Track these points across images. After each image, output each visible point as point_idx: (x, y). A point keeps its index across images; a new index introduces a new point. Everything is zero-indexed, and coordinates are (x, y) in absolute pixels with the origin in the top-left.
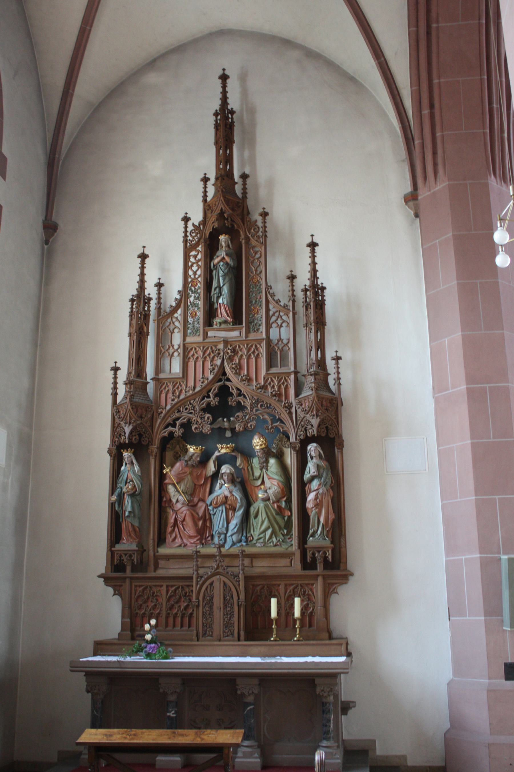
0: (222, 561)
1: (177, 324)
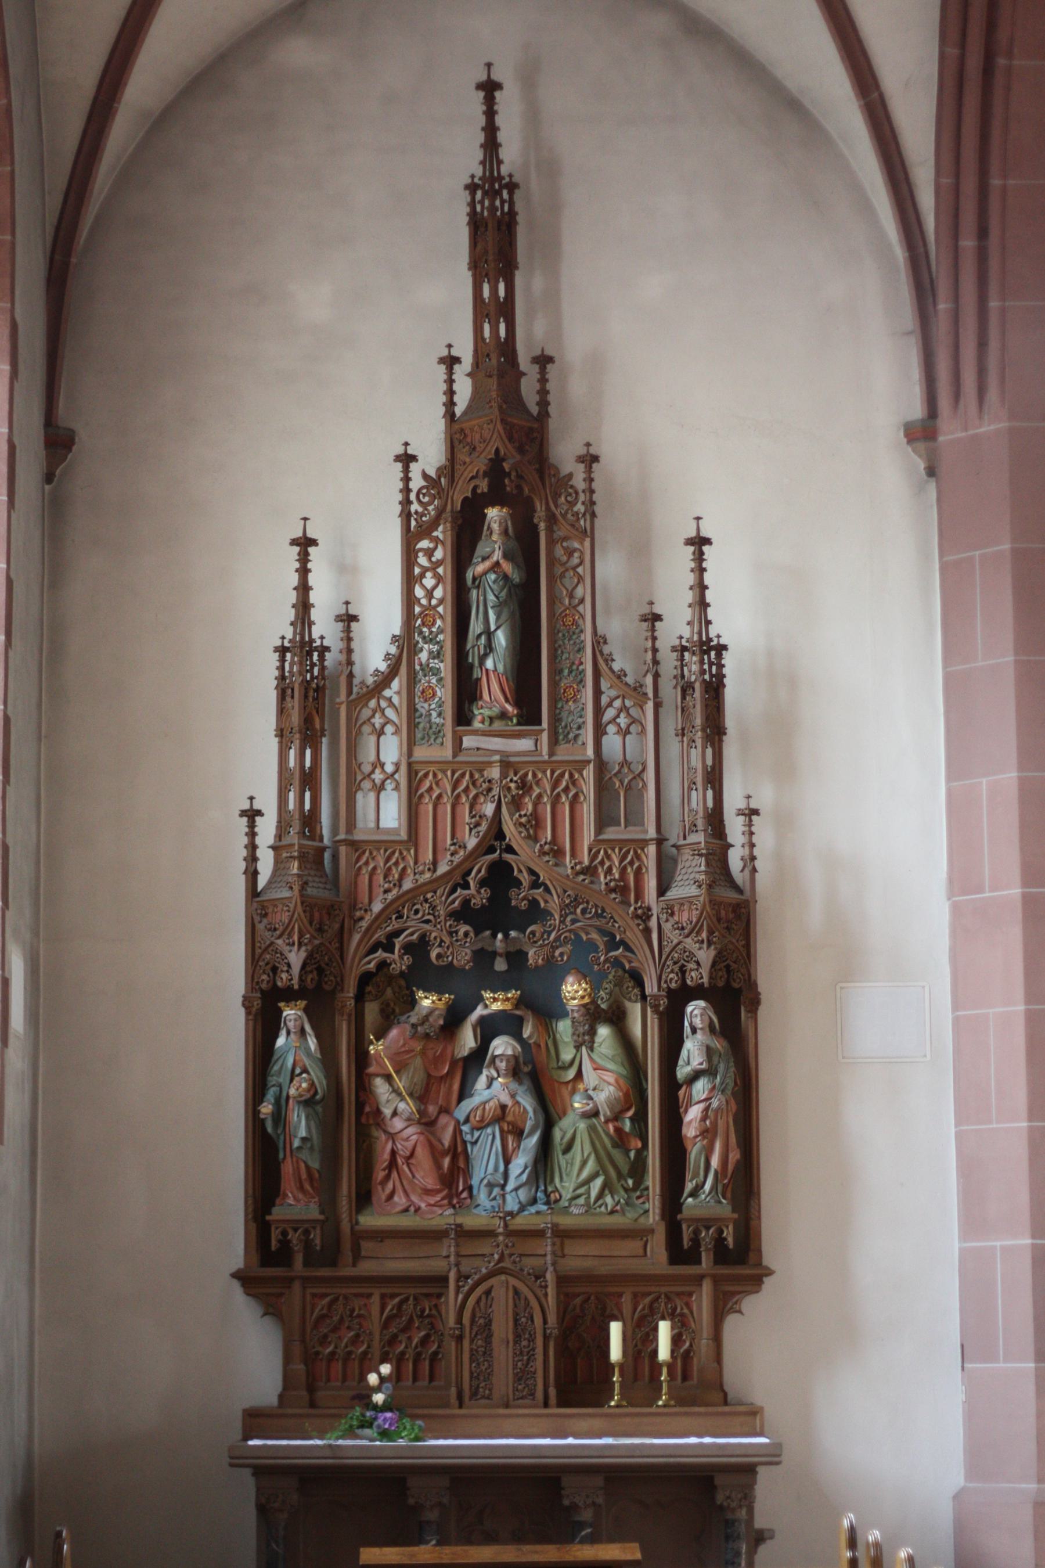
0: (510, 1244)
1: (390, 713)
